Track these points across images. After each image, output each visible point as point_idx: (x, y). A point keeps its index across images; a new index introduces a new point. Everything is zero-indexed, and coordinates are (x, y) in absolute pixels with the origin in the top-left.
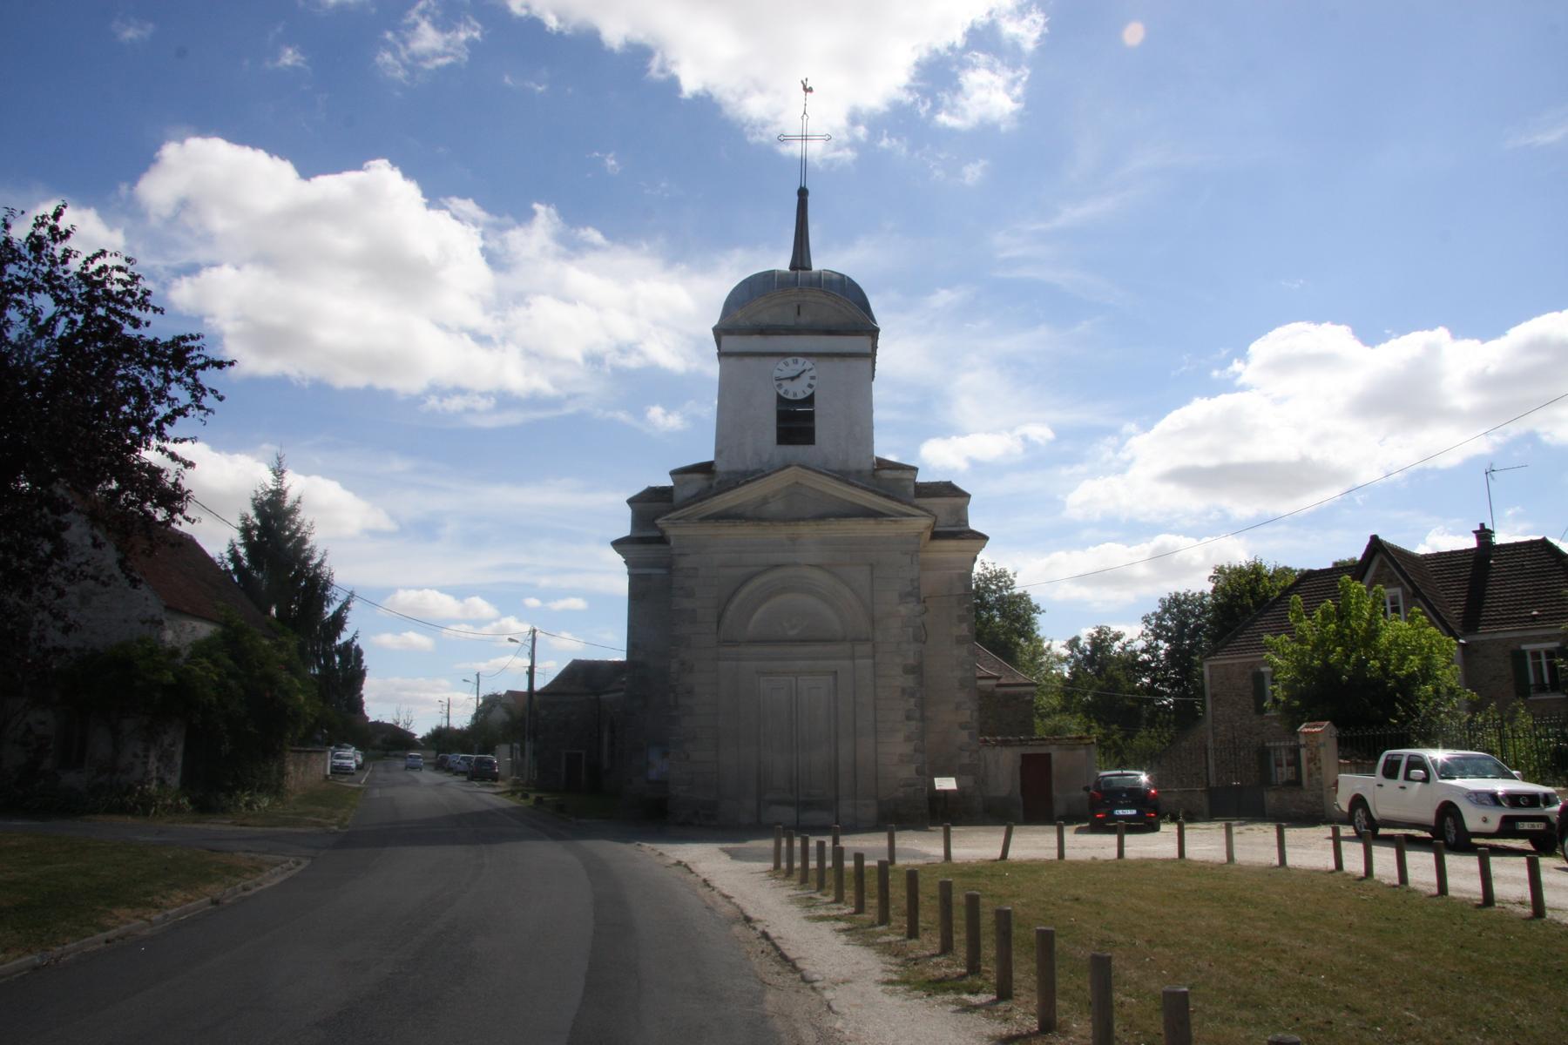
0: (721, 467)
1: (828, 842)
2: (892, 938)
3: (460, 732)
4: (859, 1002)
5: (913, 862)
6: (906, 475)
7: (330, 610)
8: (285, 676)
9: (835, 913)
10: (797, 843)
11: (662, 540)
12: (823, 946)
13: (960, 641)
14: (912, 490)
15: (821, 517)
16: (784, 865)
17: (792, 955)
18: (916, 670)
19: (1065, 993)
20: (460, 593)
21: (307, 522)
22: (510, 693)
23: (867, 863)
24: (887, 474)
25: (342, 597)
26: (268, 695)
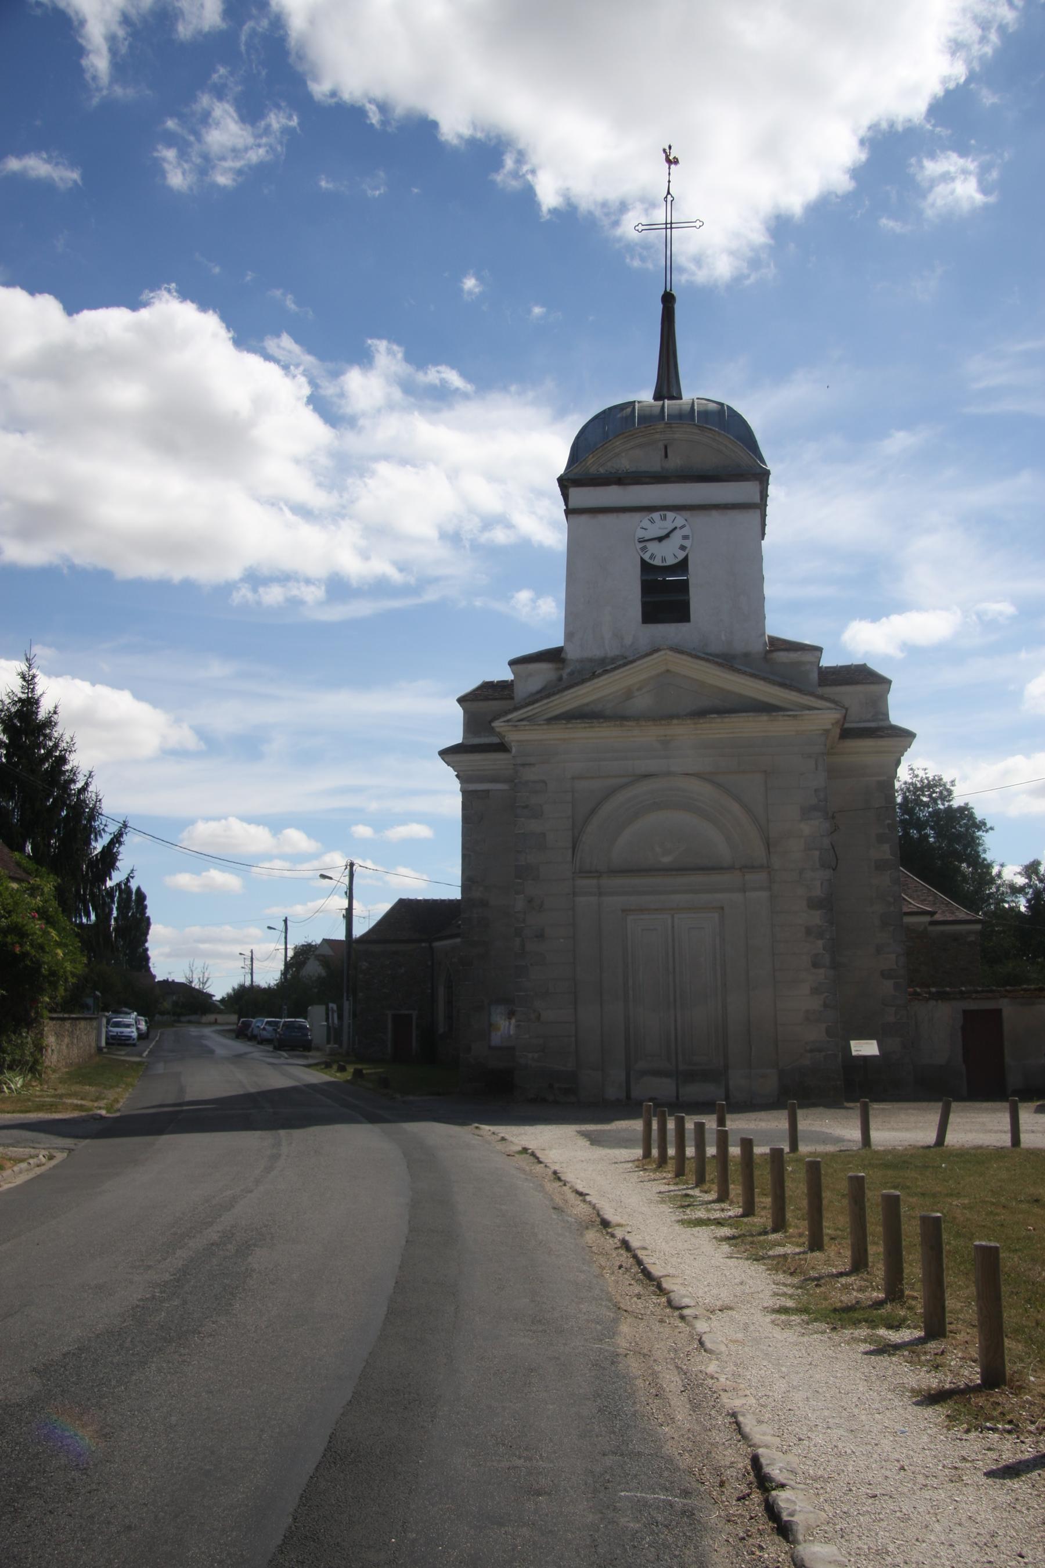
0: (572, 654)
1: (710, 1123)
2: (789, 1249)
3: (268, 991)
4: (740, 1336)
5: (821, 1148)
6: (808, 657)
7: (98, 846)
8: (38, 925)
9: (717, 1215)
10: (671, 1125)
11: (502, 747)
12: (698, 1260)
13: (881, 866)
14: (814, 676)
15: (701, 714)
16: (655, 1152)
17: (656, 1271)
18: (826, 904)
19: (1018, 1330)
20: (276, 824)
21: (67, 738)
22: (326, 941)
23: (758, 1150)
24: (782, 657)
25: (113, 828)
26: (18, 950)
